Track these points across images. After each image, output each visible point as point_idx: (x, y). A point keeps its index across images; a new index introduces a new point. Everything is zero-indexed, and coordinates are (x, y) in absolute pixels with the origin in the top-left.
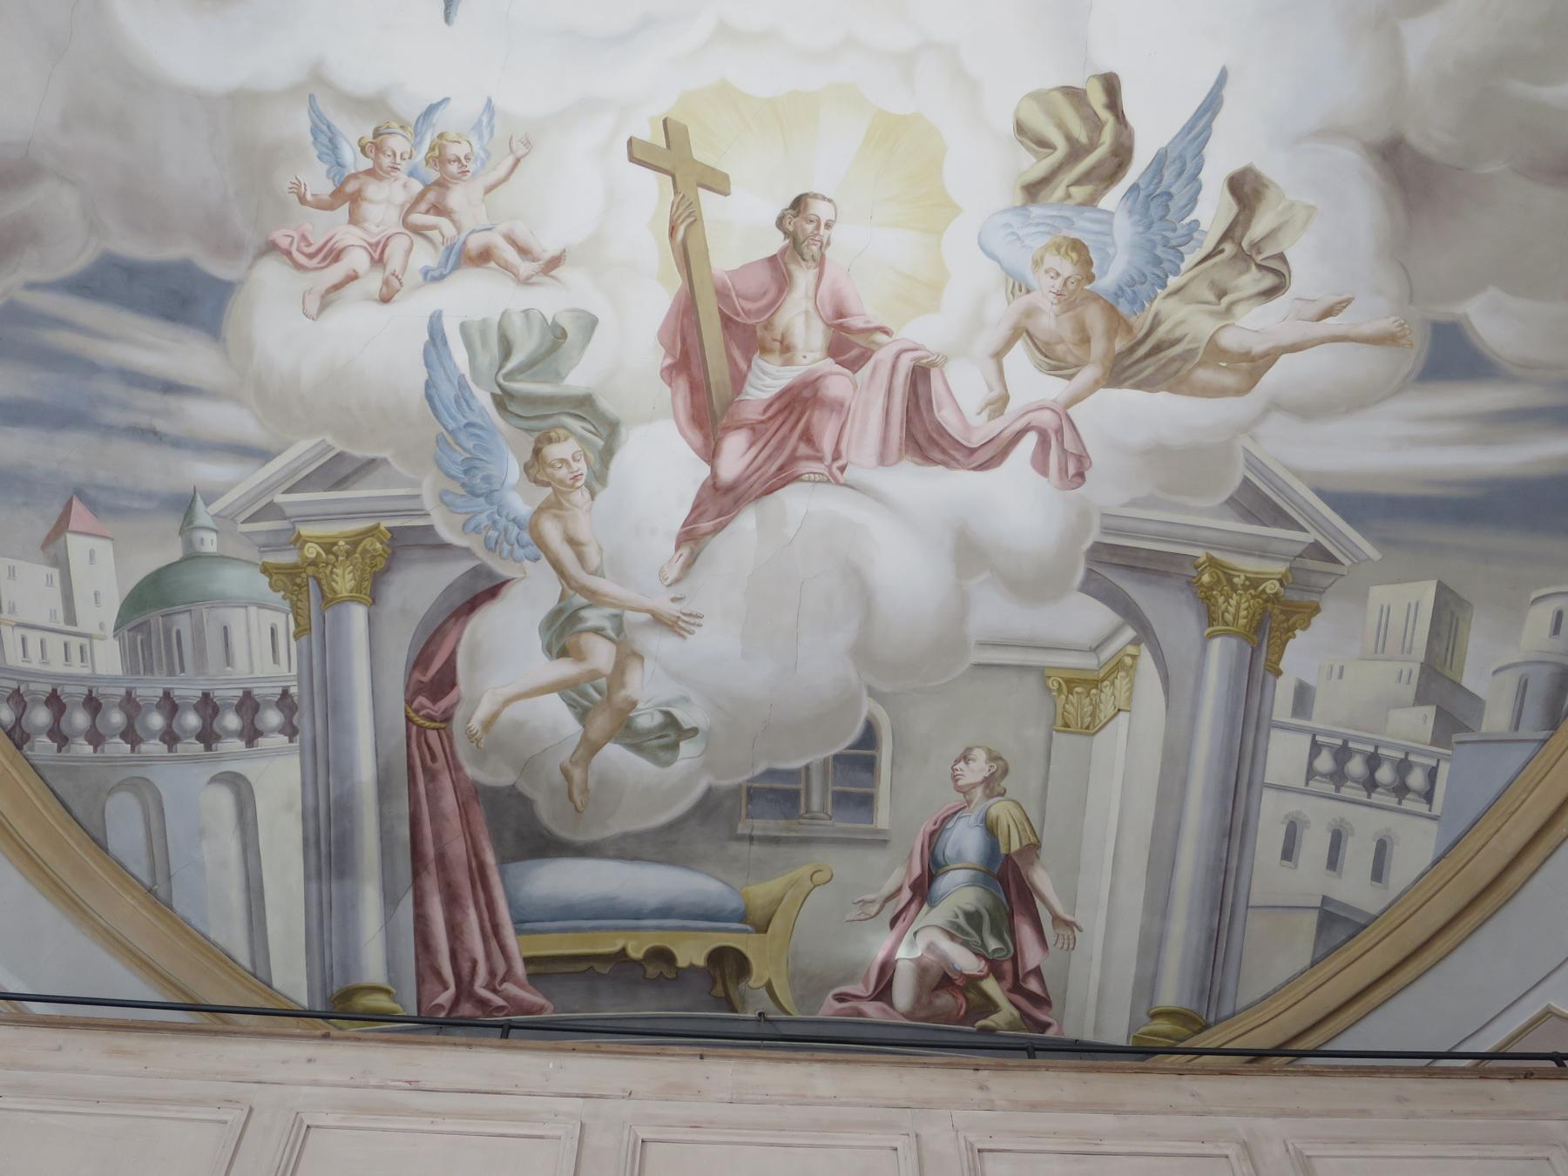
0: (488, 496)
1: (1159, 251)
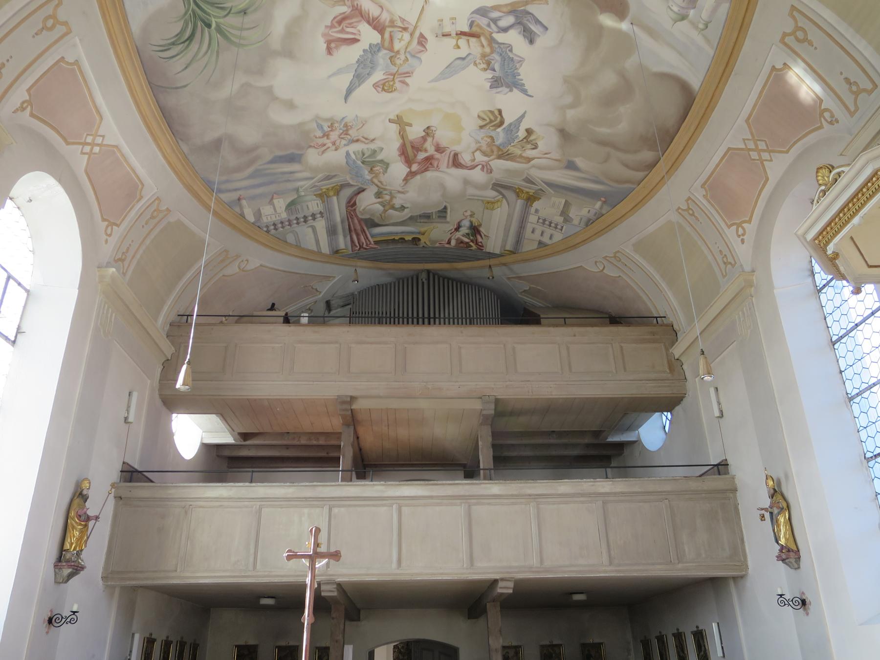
0: (361, 177)
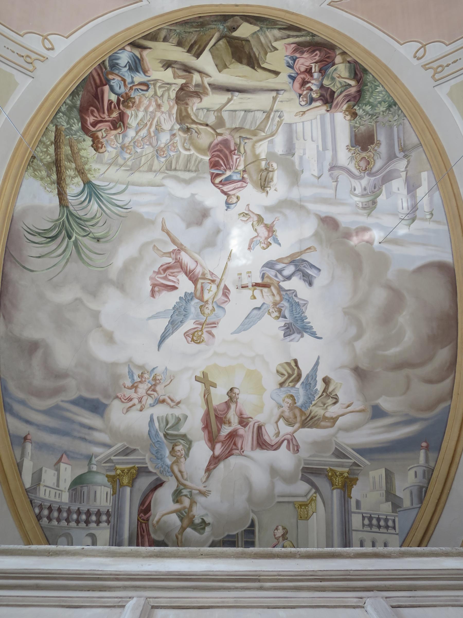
0: (161, 459)
1: (310, 396)
